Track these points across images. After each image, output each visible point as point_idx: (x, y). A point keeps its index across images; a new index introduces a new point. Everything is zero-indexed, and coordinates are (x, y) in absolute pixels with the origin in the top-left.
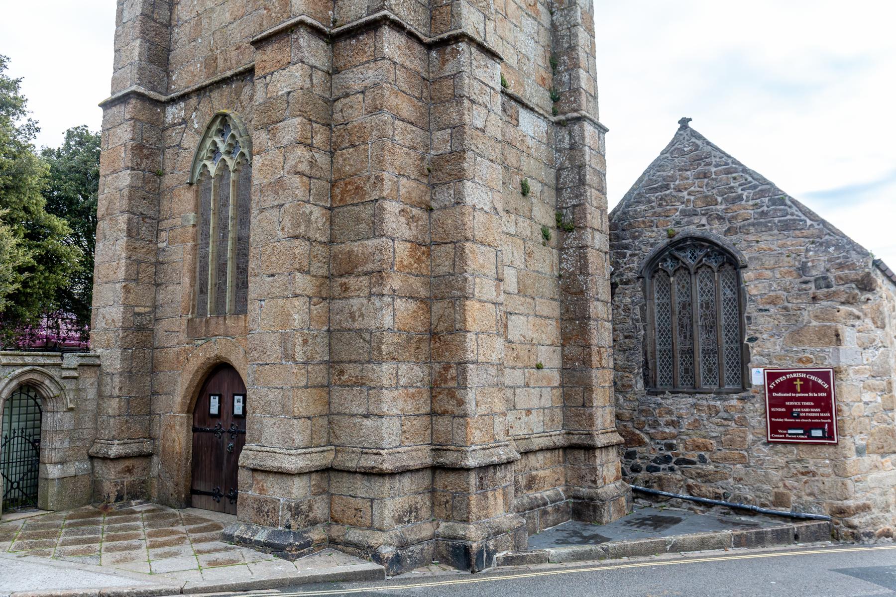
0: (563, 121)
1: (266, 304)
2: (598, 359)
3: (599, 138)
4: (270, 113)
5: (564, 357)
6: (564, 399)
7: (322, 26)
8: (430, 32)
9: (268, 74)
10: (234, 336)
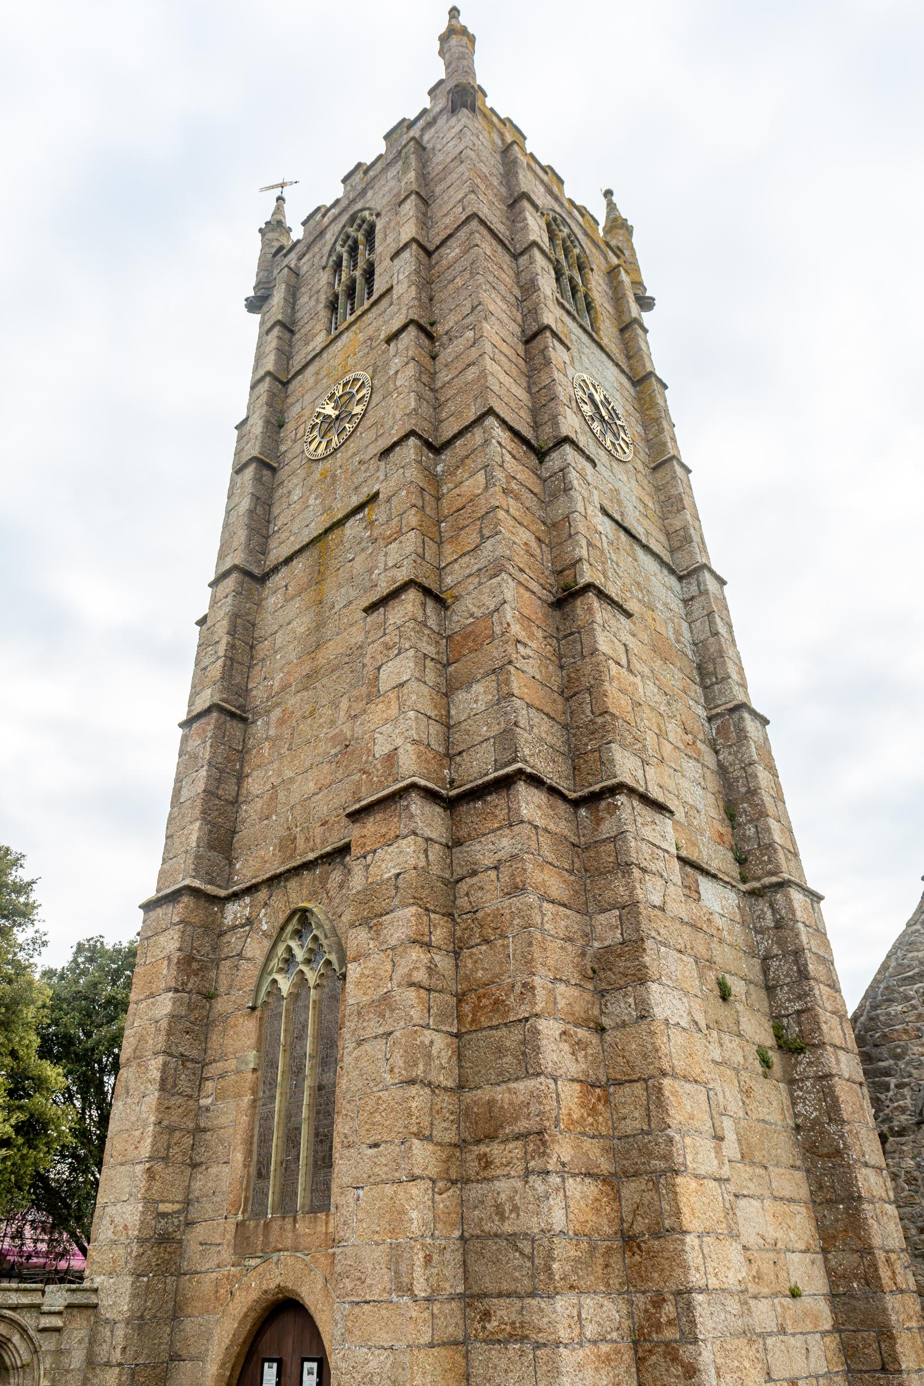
0: (759, 889)
1: (365, 1195)
2: (889, 1273)
3: (813, 909)
4: (372, 904)
5: (830, 1272)
6: (846, 1357)
7: (437, 789)
8: (575, 785)
9: (369, 853)
10: (307, 1250)
